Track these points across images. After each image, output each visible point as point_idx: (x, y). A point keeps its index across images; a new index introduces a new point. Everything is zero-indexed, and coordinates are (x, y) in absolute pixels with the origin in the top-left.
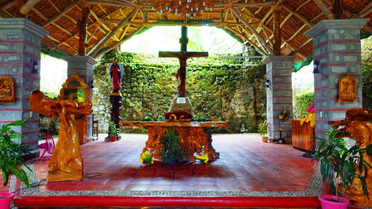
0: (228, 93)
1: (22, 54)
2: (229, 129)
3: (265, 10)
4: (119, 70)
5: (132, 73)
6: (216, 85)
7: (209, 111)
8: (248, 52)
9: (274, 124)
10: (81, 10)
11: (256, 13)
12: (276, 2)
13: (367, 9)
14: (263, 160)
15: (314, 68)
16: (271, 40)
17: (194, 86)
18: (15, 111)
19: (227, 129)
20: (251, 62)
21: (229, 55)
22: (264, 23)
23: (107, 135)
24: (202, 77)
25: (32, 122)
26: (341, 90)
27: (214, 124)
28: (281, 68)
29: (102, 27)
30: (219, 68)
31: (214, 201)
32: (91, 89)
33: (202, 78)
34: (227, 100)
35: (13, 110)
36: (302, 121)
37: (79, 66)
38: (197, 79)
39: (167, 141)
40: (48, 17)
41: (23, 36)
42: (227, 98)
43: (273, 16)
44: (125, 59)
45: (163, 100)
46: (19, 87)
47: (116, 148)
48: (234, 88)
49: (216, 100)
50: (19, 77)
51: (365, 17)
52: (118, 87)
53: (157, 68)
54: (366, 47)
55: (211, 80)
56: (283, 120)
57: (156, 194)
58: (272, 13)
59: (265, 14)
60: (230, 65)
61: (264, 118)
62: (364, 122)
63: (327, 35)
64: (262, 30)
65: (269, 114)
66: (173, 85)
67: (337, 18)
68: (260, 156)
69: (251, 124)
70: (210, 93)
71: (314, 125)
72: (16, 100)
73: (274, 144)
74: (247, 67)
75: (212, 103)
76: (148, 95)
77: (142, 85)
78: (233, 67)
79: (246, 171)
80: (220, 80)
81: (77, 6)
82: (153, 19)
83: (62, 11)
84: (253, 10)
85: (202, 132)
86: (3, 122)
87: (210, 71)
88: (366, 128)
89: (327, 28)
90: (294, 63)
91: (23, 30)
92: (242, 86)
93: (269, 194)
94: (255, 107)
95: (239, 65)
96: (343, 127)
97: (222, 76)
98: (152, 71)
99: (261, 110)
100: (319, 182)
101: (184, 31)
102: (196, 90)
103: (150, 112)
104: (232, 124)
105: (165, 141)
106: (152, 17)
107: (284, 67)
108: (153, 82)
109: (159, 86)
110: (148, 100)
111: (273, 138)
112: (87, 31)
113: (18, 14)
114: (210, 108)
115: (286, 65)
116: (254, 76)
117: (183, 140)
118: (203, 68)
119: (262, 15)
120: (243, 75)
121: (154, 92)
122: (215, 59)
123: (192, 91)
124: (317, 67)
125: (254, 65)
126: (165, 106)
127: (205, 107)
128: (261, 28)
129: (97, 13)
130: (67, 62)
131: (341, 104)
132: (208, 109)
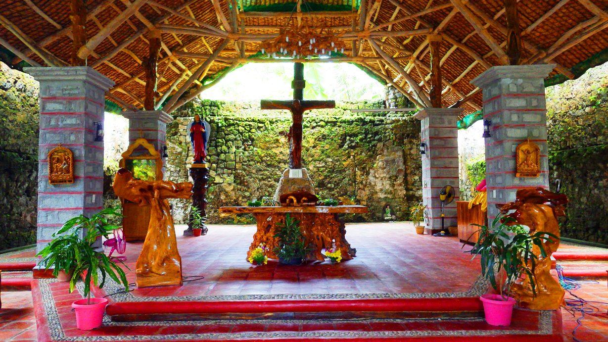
0: (364, 162)
1: (83, 115)
3: (418, 40)
4: (203, 130)
5: (218, 132)
6: (347, 149)
7: (336, 189)
8: (394, 99)
9: (433, 208)
11: (405, 42)
12: (434, 30)
13: (284, 332)
14: (416, 258)
15: (485, 130)
16: (428, 82)
17: (313, 151)
18: (73, 195)
19: (364, 215)
20: (399, 114)
21: (366, 103)
22: (418, 58)
23: (186, 227)
24: (324, 137)
25: (94, 209)
26: (520, 161)
29: (174, 64)
30: (350, 123)
31: (353, 304)
32: (163, 158)
33: (325, 139)
34: (364, 172)
35: (71, 193)
36: (471, 201)
38: (318, 141)
39: (285, 232)
40: (99, 54)
42: (364, 168)
43: (429, 49)
44: (207, 110)
45: (266, 172)
46: (80, 161)
47: (204, 246)
48: (374, 153)
49: (347, 172)
50: (79, 147)
52: (202, 155)
54: (562, 96)
55: (339, 141)
56: (446, 201)
57: (282, 298)
59: (419, 45)
60: (368, 119)
61: (419, 199)
63: (500, 85)
64: (414, 67)
65: (426, 194)
66: (282, 150)
67: (513, 63)
68: (411, 253)
69: (400, 208)
71: (486, 209)
72: (75, 179)
73: (433, 237)
74: (393, 122)
75: (340, 177)
76: (243, 165)
77: (234, 149)
78: (371, 121)
79: (393, 271)
80: (352, 141)
81: (141, 36)
82: (251, 51)
83: (120, 43)
84: (400, 40)
85: (331, 221)
86: (57, 209)
87: (337, 128)
88: (541, 213)
89: (500, 76)
90: (463, 115)
93: (422, 296)
94: (406, 181)
95: (381, 118)
96: (514, 211)
97: (355, 135)
98: (248, 129)
99: (415, 186)
100: (486, 282)
101: (299, 69)
102: (316, 157)
103: (246, 191)
104: (372, 207)
105: (283, 234)
106: (249, 48)
108: (250, 145)
109: (259, 150)
110: (243, 172)
111: (431, 228)
112: (158, 75)
113: (74, 59)
115: (450, 122)
116: (403, 134)
117: (307, 231)
118: (327, 123)
119: (414, 46)
120: (387, 134)
121: (252, 160)
122: (345, 110)
123: (310, 159)
124: (488, 129)
125: (404, 118)
126: (270, 181)
127: (330, 183)
128: (413, 65)
129: (169, 44)
130: (128, 120)
131: (520, 179)
132: (335, 186)
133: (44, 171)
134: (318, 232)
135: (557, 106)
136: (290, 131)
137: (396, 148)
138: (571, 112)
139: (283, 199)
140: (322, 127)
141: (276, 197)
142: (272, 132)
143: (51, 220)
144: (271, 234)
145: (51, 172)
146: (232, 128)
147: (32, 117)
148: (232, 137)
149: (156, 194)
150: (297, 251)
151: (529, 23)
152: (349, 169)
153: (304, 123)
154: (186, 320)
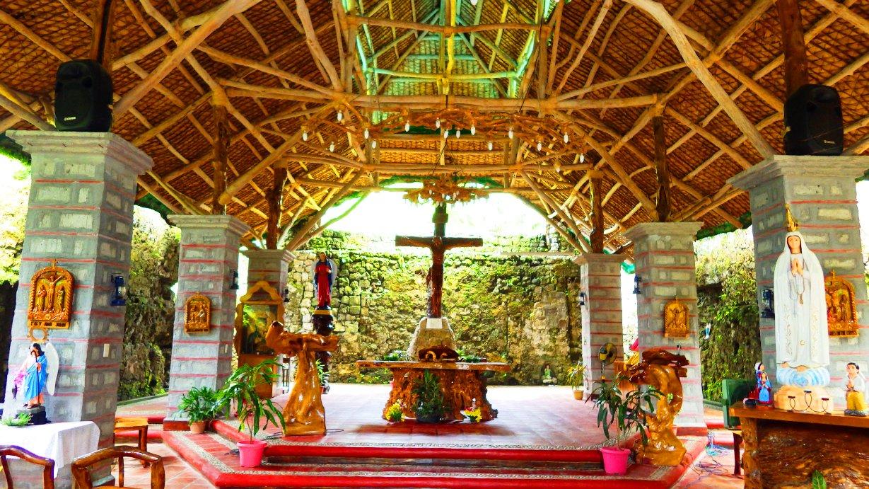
0: (518, 310)
2: (520, 376)
9: (593, 369)
10: (273, 172)
12: (594, 165)
17: (455, 295)
18: (208, 345)
22: (580, 191)
24: (470, 278)
26: (668, 320)
27: (489, 366)
28: (602, 274)
29: (295, 191)
30: (502, 262)
33: (471, 280)
37: (268, 267)
39: (423, 389)
41: (225, 238)
42: (518, 318)
43: (590, 185)
44: (329, 243)
45: (398, 320)
48: (530, 299)
49: (497, 322)
50: (217, 296)
51: (699, 220)
53: (387, 260)
58: (587, 182)
62: (663, 366)
65: (586, 351)
70: (486, 308)
72: (211, 327)
74: (554, 262)
75: (489, 327)
77: (359, 291)
78: (527, 261)
80: (504, 285)
83: (242, 173)
89: (647, 233)
91: (226, 230)
92: (545, 297)
94: (569, 336)
97: (508, 277)
98: (378, 266)
102: (460, 303)
103: (372, 342)
107: (608, 272)
110: (370, 319)
114: (485, 337)
115: (612, 271)
116: (567, 278)
118: (474, 261)
120: (547, 276)
121: (381, 305)
123: (452, 305)
126: (401, 331)
127: (475, 335)
128: (576, 198)
131: (669, 340)
132: (482, 339)
133: (181, 319)
134: (458, 390)
135: (733, 256)
136: (430, 273)
137: (557, 295)
138: (745, 264)
139: (422, 354)
140: (468, 265)
141: (410, 351)
142: (406, 271)
143: (184, 369)
144: (408, 391)
145: (189, 319)
146: (358, 264)
147: (142, 253)
148: (357, 275)
149: (304, 345)
150: (435, 408)
151: (691, 169)
152: (500, 319)
153: (446, 261)
154: (334, 463)
